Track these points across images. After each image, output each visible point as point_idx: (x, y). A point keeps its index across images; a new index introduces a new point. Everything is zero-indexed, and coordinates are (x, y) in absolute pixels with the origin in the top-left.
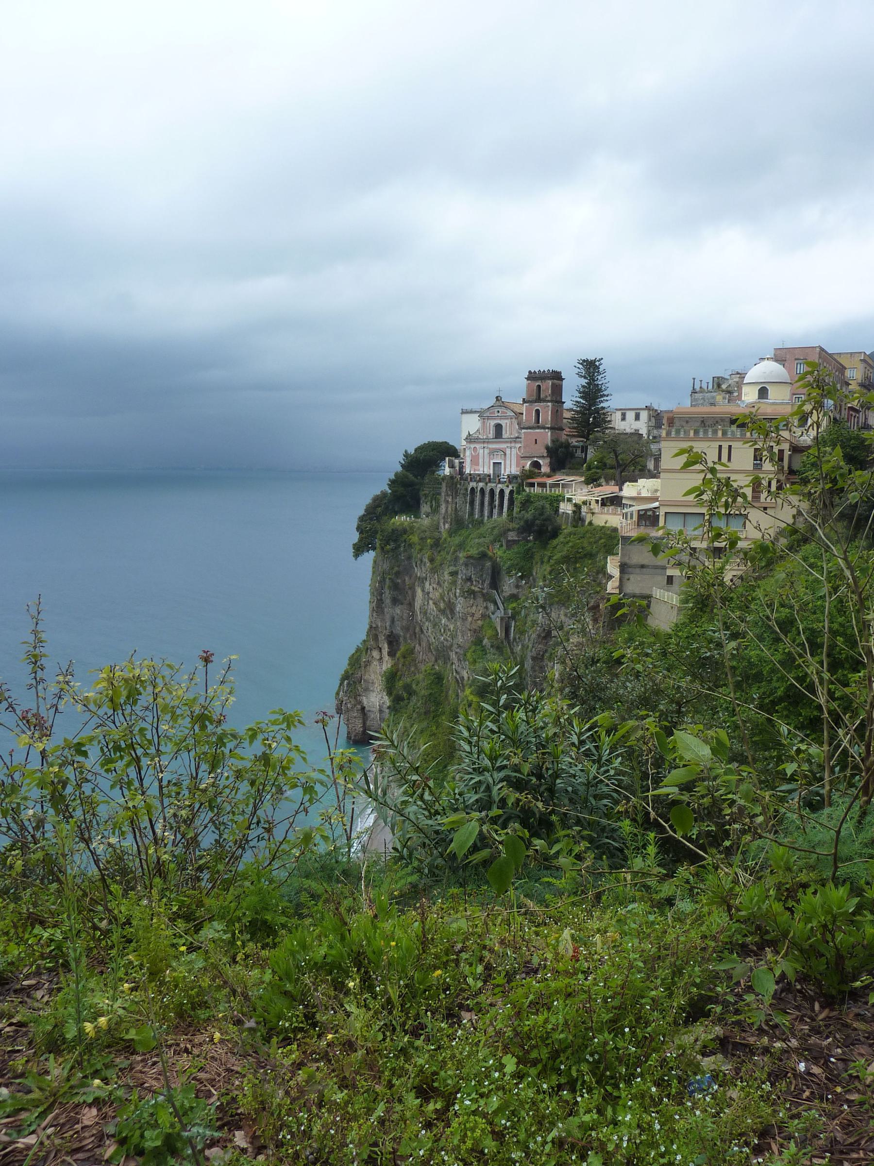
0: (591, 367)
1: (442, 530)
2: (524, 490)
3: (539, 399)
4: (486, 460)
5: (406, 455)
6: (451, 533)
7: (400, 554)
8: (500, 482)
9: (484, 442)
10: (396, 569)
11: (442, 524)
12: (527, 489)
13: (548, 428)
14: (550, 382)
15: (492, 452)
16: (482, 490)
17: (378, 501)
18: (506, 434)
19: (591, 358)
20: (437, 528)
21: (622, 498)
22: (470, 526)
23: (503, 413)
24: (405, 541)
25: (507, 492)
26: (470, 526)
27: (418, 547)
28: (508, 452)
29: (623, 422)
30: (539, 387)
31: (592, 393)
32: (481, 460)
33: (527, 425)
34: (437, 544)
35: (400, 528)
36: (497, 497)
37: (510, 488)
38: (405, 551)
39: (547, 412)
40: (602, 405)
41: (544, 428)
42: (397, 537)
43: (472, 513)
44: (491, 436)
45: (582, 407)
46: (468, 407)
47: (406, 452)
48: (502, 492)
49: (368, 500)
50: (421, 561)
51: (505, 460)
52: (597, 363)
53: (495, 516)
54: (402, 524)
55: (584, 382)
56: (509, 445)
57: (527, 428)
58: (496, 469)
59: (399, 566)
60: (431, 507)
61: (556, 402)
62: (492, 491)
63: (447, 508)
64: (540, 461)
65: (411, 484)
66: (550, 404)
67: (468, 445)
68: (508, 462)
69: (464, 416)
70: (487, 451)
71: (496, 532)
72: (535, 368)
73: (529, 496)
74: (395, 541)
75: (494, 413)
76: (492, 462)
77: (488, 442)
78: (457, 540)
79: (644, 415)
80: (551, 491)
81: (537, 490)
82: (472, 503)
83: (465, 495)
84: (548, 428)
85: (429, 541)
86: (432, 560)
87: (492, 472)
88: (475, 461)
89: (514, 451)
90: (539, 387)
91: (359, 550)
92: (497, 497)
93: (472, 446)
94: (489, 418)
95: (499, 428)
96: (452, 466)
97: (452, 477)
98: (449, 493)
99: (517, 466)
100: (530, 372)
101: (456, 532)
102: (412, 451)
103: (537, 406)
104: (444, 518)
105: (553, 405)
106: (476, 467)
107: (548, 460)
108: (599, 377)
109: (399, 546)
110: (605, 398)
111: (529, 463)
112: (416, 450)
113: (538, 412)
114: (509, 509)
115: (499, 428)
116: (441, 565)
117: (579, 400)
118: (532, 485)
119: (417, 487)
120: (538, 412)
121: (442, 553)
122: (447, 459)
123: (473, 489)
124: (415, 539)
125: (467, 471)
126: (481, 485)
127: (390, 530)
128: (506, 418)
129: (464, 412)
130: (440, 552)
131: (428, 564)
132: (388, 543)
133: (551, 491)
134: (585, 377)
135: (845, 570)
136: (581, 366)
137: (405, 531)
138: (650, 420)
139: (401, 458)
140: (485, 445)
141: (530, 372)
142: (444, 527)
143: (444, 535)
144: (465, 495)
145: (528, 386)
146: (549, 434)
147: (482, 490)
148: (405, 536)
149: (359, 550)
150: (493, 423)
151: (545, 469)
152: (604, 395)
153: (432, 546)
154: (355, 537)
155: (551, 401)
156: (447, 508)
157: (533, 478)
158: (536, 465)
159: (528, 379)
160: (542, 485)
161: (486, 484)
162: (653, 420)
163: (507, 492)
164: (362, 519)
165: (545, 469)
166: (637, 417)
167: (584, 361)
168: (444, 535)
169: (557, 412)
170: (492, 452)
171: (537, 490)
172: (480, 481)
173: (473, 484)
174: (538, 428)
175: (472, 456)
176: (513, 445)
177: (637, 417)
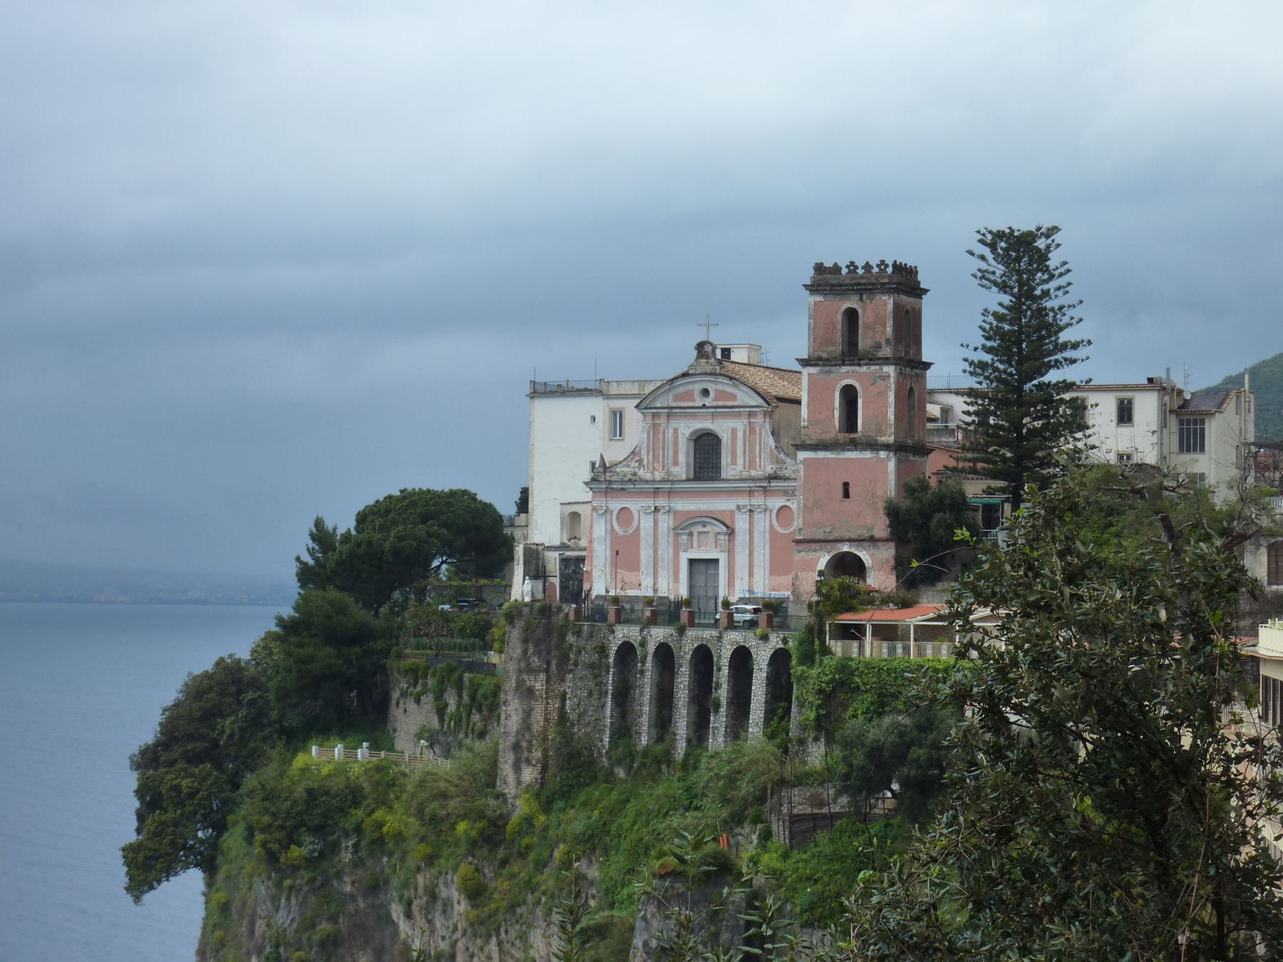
1: (510, 790)
2: (826, 651)
3: (851, 353)
4: (666, 551)
5: (321, 536)
6: (546, 798)
7: (339, 875)
8: (732, 625)
9: (656, 493)
10: (325, 927)
11: (506, 769)
12: (837, 647)
13: (887, 447)
14: (888, 302)
15: (686, 526)
16: (665, 655)
17: (216, 694)
18: (732, 467)
19: (1024, 225)
20: (490, 778)
21: (1256, 660)
22: (621, 772)
23: (720, 395)
24: (358, 830)
25: (762, 657)
26: (621, 772)
27: (417, 851)
28: (741, 523)
29: (1125, 430)
30: (851, 315)
31: (1026, 335)
32: (645, 554)
33: (814, 436)
34: (492, 834)
35: (338, 784)
36: (723, 676)
37: (775, 641)
38: (358, 863)
39: (883, 394)
41: (873, 446)
42: (322, 817)
43: (623, 730)
44: (681, 470)
45: (999, 380)
46: (552, 377)
47: (319, 523)
48: (742, 658)
49: (170, 693)
50: (433, 896)
51: (731, 552)
52: (1041, 243)
53: (717, 739)
54: (341, 770)
55: (997, 300)
56: (744, 501)
57: (815, 447)
58: (700, 580)
59: (333, 918)
60: (441, 711)
62: (703, 657)
63: (528, 713)
64: (864, 555)
65: (361, 636)
66: (890, 370)
67: (600, 502)
68: (741, 558)
69: (545, 409)
70: (665, 522)
71: (745, 788)
72: (836, 256)
73: (844, 667)
74: (319, 830)
75: (689, 396)
76: (684, 557)
77: (670, 493)
78: (576, 821)
79: (1147, 407)
80: (920, 652)
81: (871, 649)
82: (624, 696)
83: (597, 669)
84: (887, 447)
85: (462, 827)
86: (475, 893)
88: (624, 554)
90: (851, 315)
91: (146, 867)
92: (723, 676)
93: (615, 505)
94: (671, 412)
95: (706, 452)
98: (536, 661)
100: (819, 268)
101: (566, 793)
102: (343, 522)
103: (848, 375)
104: (516, 747)
105: (900, 374)
106: (629, 576)
107: (888, 552)
108: (1052, 285)
109: (335, 848)
110: (1069, 354)
112: (362, 518)
113: (849, 395)
114: (770, 713)
115: (706, 452)
116: (512, 908)
117: (987, 358)
118: (851, 633)
119: (379, 645)
120: (849, 395)
121: (515, 867)
124: (394, 820)
125: (599, 584)
126: (659, 634)
127: (300, 791)
128: (732, 411)
129: (540, 391)
130: (504, 863)
131: (461, 907)
132: (291, 839)
133: (920, 652)
134: (1003, 287)
136: (986, 251)
137: (354, 796)
138: (1164, 424)
139: (301, 546)
140: (662, 502)
141: (819, 268)
142: (517, 783)
143: (521, 807)
144: (597, 669)
145: (816, 311)
146: (891, 465)
147: (665, 655)
148: (360, 813)
149: (146, 867)
150: (686, 428)
151: (880, 578)
152: (1064, 347)
153: (473, 846)
155: (896, 361)
156: (528, 713)
157: (851, 609)
158: (848, 566)
159: (813, 288)
160: (887, 633)
161: (681, 631)
162: (1173, 421)
163: (762, 657)
164: (148, 760)
165: (880, 578)
166: (1125, 414)
167: (999, 235)
168: (521, 807)
169: (912, 397)
170: (686, 526)
171: (871, 649)
172: (653, 621)
173: (623, 633)
174: (855, 445)
176: (757, 500)
177: (1125, 414)
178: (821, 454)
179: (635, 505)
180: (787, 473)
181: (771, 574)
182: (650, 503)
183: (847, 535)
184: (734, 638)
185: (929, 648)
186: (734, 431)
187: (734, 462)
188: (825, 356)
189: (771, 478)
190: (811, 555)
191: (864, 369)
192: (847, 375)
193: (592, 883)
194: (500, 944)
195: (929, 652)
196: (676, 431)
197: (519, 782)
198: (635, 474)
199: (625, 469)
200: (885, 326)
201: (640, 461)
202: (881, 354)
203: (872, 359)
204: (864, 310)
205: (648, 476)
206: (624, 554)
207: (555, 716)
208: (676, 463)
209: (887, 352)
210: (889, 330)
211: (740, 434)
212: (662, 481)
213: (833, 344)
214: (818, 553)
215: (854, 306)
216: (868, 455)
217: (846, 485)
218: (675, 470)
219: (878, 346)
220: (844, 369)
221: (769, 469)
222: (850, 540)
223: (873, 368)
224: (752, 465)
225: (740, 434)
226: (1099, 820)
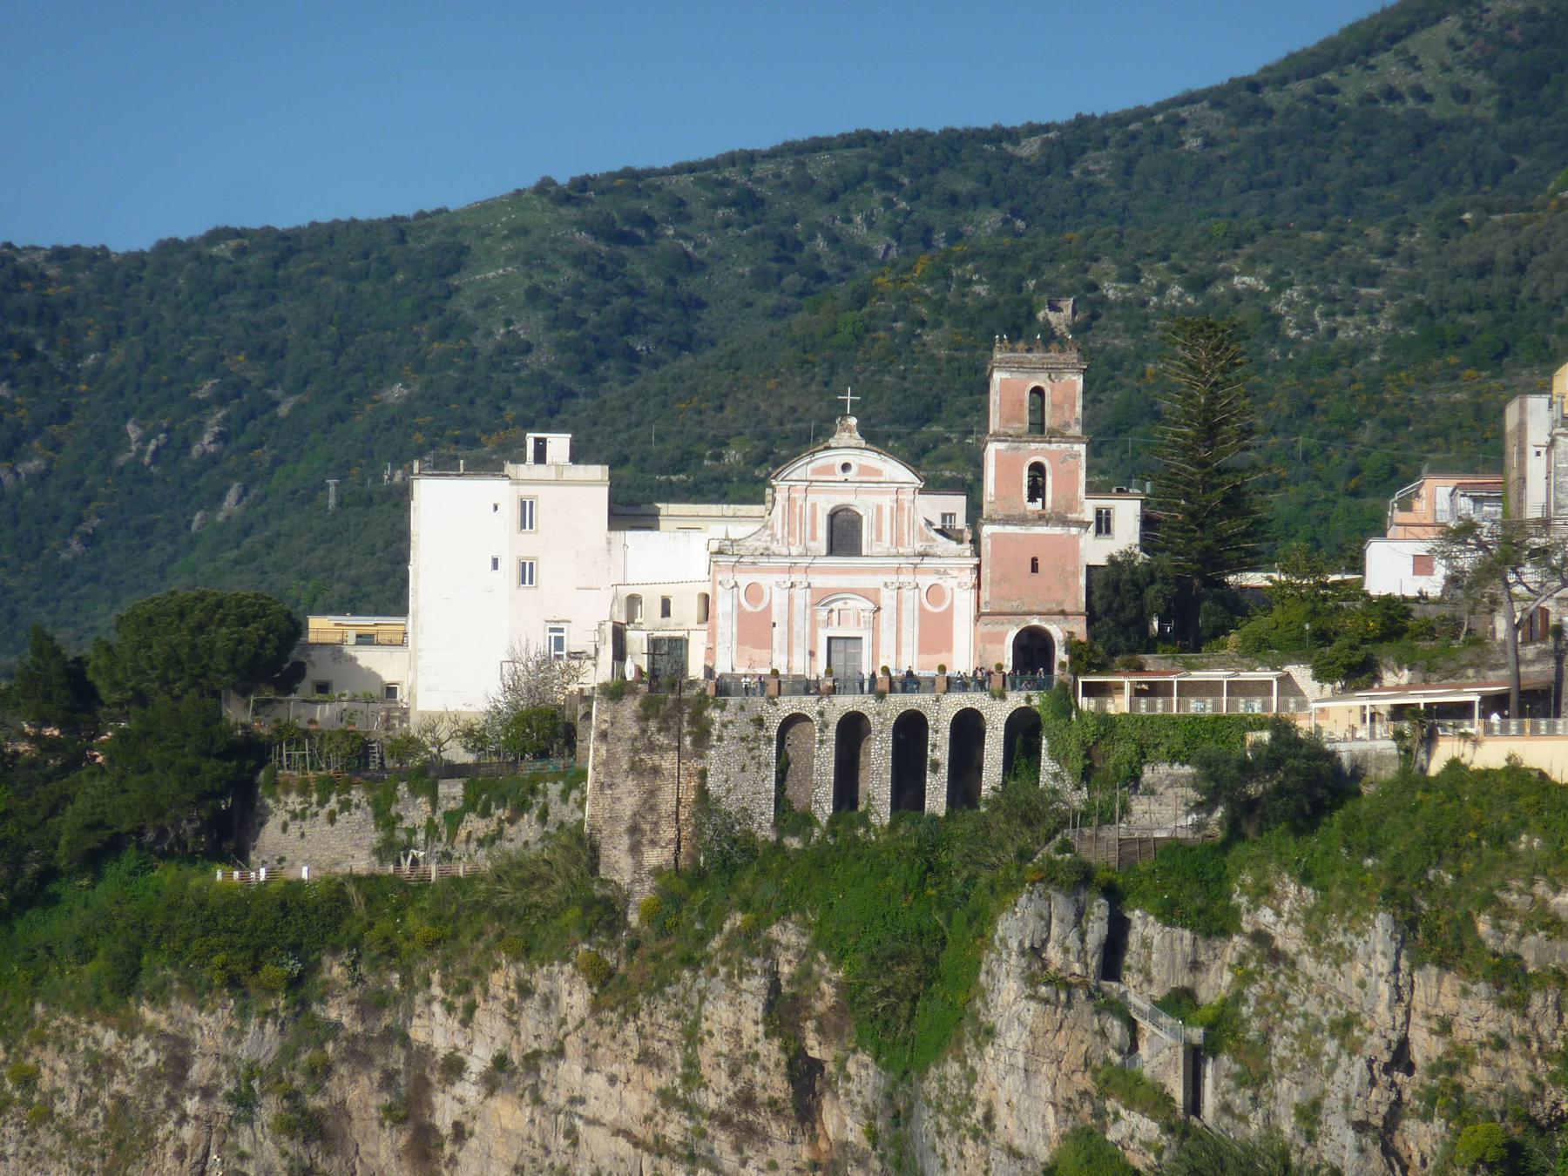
3: (1038, 427)
4: (801, 627)
23: (864, 470)
28: (887, 599)
39: (1075, 472)
48: (968, 728)
51: (875, 630)
70: (802, 598)
89: (911, 600)
93: (744, 580)
103: (1036, 451)
111: (1016, 631)
113: (1037, 470)
120: (1037, 470)
174: (1042, 519)
176: (906, 578)
178: (1009, 529)
179: (766, 581)
180: (939, 551)
181: (921, 652)
182: (786, 579)
183: (1035, 609)
184: (956, 702)
185: (1143, 703)
186: (879, 508)
187: (879, 538)
188: (1011, 432)
189: (923, 555)
190: (998, 628)
191: (1054, 446)
192: (1036, 452)
193: (787, 948)
194: (639, 1031)
195: (1160, 706)
196: (814, 506)
197: (639, 866)
198: (767, 549)
199: (757, 544)
200: (1074, 406)
201: (773, 536)
202: (1070, 432)
203: (1059, 435)
204: (1052, 389)
205: (785, 551)
206: (755, 629)
207: (692, 795)
208: (814, 538)
209: (1077, 430)
210: (1079, 409)
211: (886, 511)
212: (800, 555)
213: (1020, 420)
214: (1006, 627)
215: (1042, 385)
216: (1058, 530)
217: (1034, 560)
218: (811, 545)
219: (1068, 425)
220: (1033, 446)
221: (919, 547)
222: (1039, 614)
223: (1063, 446)
224: (898, 541)
225: (886, 511)
226: (751, 1118)
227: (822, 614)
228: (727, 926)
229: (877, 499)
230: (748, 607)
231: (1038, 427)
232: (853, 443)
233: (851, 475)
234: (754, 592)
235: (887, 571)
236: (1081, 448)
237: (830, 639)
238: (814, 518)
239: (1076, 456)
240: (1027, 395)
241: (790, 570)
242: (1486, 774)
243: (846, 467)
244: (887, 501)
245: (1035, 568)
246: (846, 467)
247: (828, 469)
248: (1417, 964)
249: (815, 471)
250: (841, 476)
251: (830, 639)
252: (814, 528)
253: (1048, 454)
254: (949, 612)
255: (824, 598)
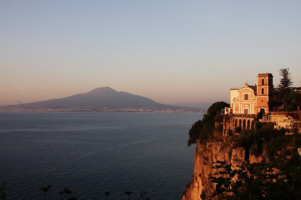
0: (285, 73)
3: (263, 84)
23: (248, 90)
28: (251, 105)
30: (263, 80)
40: (289, 86)
51: (249, 108)
55: (282, 78)
56: (251, 102)
61: (270, 85)
64: (264, 109)
69: (231, 90)
70: (242, 105)
87: (244, 113)
88: (237, 109)
89: (253, 105)
90: (263, 80)
93: (236, 103)
96: (227, 111)
97: (227, 115)
99: (255, 110)
103: (263, 87)
107: (268, 108)
111: (260, 109)
113: (263, 89)
120: (263, 89)
122: (225, 108)
123: (236, 120)
125: (234, 112)
135: (292, 112)
136: (281, 72)
154: (188, 137)
158: (262, 110)
159: (258, 77)
163: (251, 121)
173: (236, 118)
174: (263, 95)
175: (236, 107)
179: (238, 103)
187: (250, 98)
190: (258, 109)
192: (262, 87)
202: (267, 84)
208: (243, 98)
209: (268, 84)
210: (268, 81)
216: (265, 96)
217: (262, 100)
220: (262, 86)
227: (244, 107)
228: (67, 110)
229: (249, 93)
230: (236, 106)
231: (263, 84)
232: (247, 87)
233: (247, 90)
234: (237, 104)
235: (250, 101)
236: (268, 86)
237: (245, 110)
238: (243, 95)
239: (267, 87)
240: (261, 80)
241: (240, 102)
242: (291, 135)
243: (246, 89)
244: (250, 93)
245: (262, 101)
246: (246, 89)
247: (244, 90)
248: (257, 158)
249: (243, 90)
250: (246, 90)
251: (245, 110)
252: (243, 96)
253: (264, 87)
254: (238, 106)
255: (244, 104)
